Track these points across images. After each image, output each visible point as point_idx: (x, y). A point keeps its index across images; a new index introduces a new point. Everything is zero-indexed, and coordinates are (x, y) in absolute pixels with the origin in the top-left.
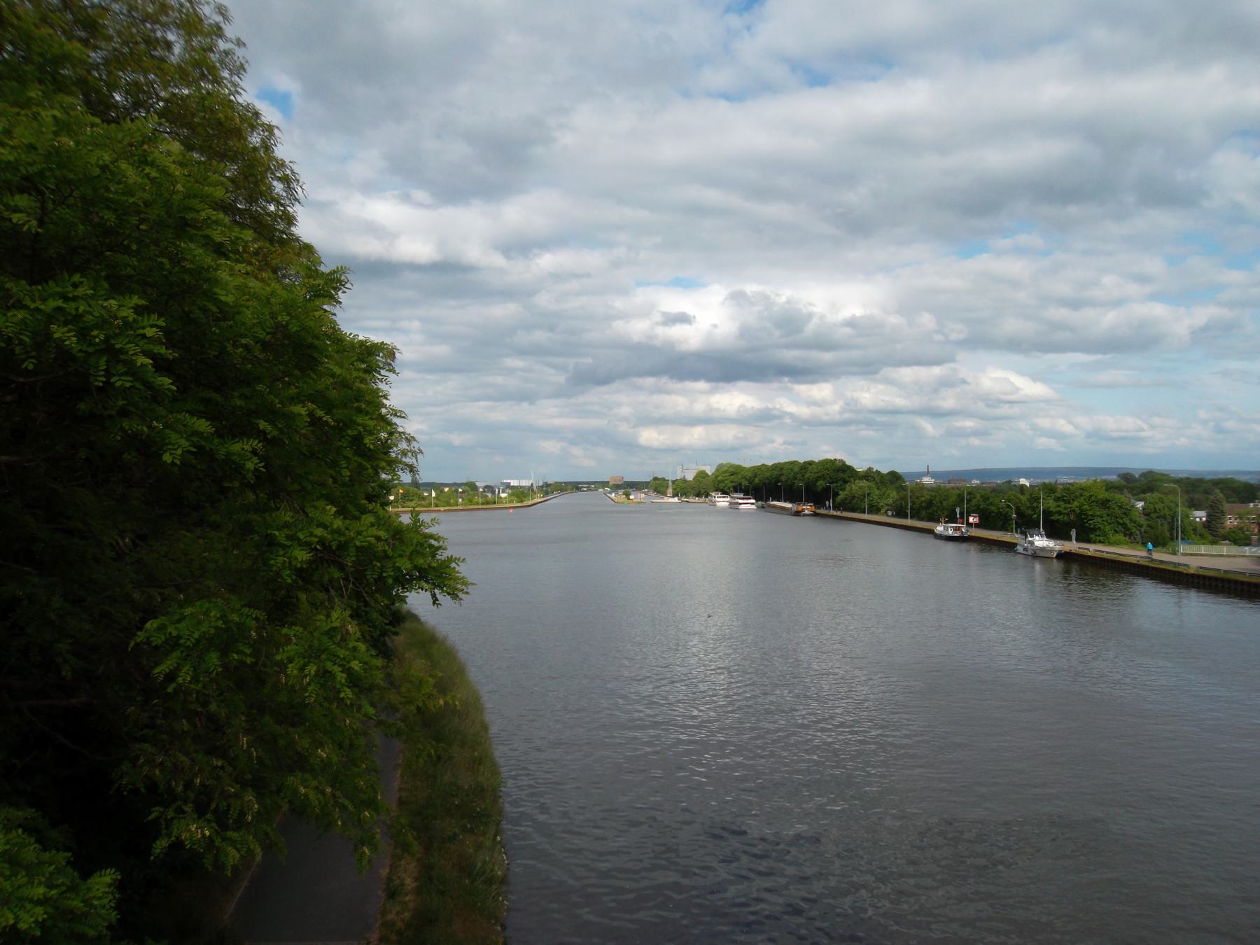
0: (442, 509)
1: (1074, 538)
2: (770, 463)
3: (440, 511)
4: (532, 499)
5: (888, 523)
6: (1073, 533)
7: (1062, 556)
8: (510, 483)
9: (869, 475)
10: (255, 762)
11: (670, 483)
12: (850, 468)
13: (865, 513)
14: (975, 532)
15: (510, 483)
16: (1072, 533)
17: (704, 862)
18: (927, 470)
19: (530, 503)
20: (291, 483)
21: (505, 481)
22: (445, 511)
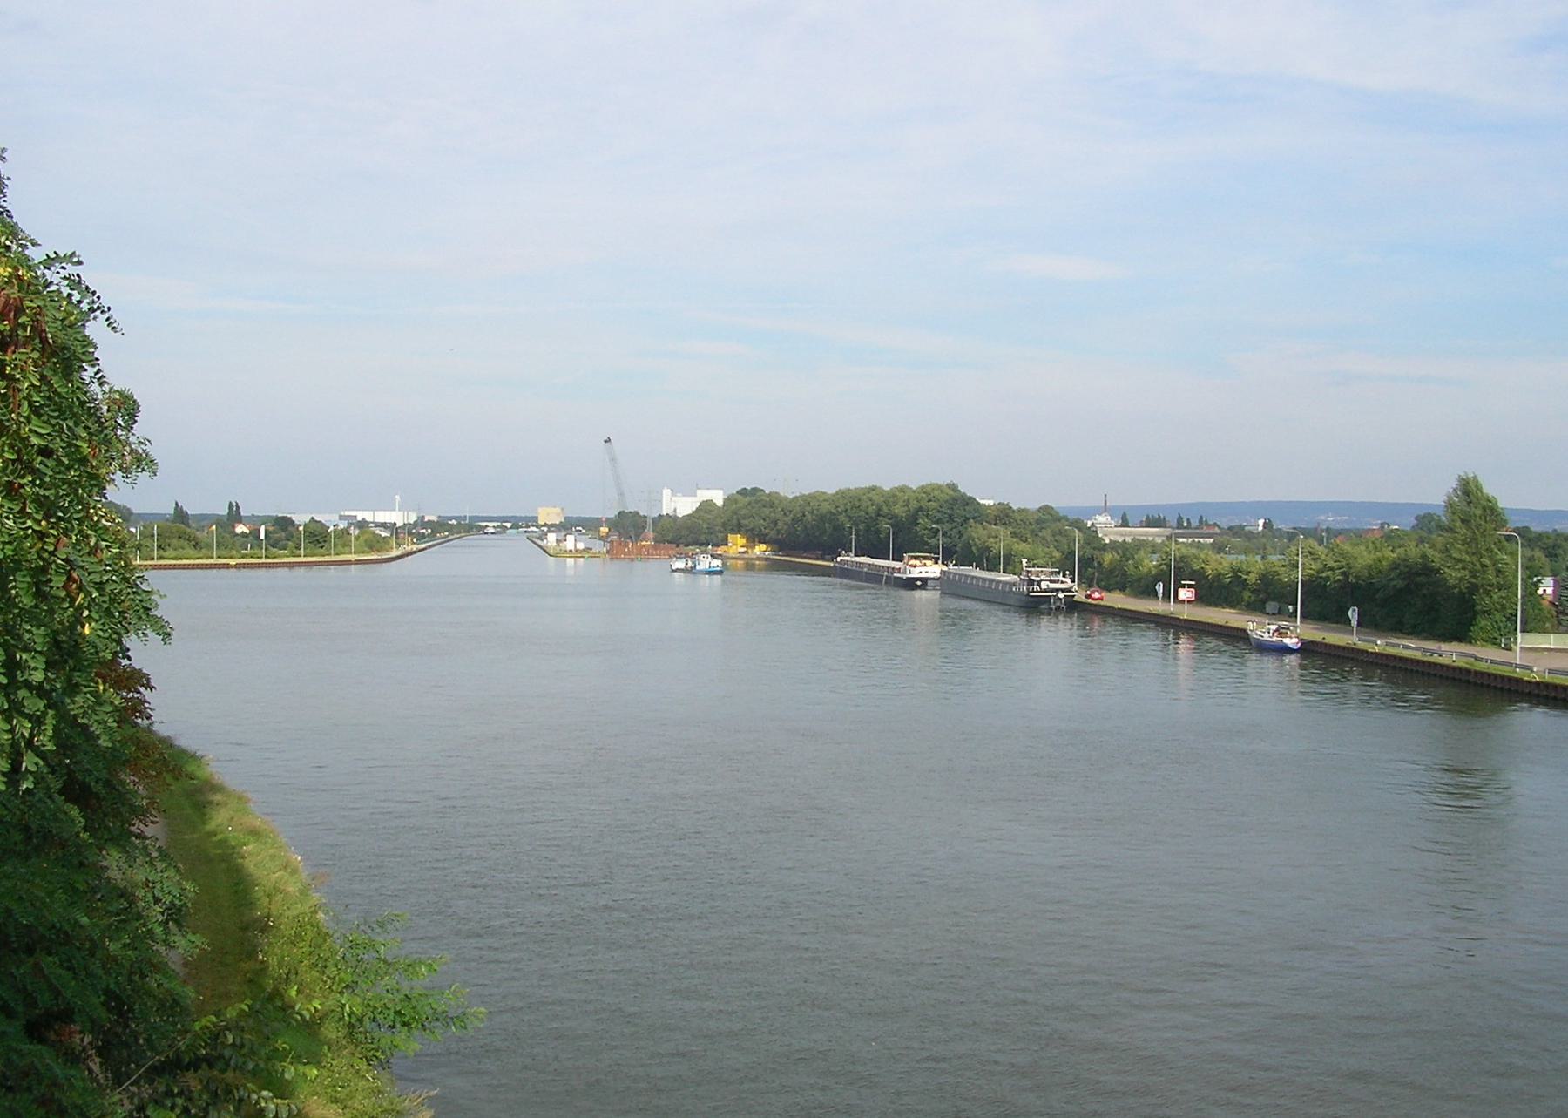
0: (232, 562)
1: (1354, 623)
2: (831, 490)
3: (228, 566)
4: (399, 545)
5: (367, 563)
6: (1353, 614)
7: (1307, 649)
8: (356, 517)
9: (1004, 515)
10: (144, 929)
11: (650, 522)
12: (969, 501)
13: (394, 510)
14: (1186, 613)
15: (356, 517)
16: (1350, 613)
17: (1307, 706)
18: (1103, 505)
19: (394, 553)
20: (1015, 586)
21: (347, 513)
22: (238, 566)
